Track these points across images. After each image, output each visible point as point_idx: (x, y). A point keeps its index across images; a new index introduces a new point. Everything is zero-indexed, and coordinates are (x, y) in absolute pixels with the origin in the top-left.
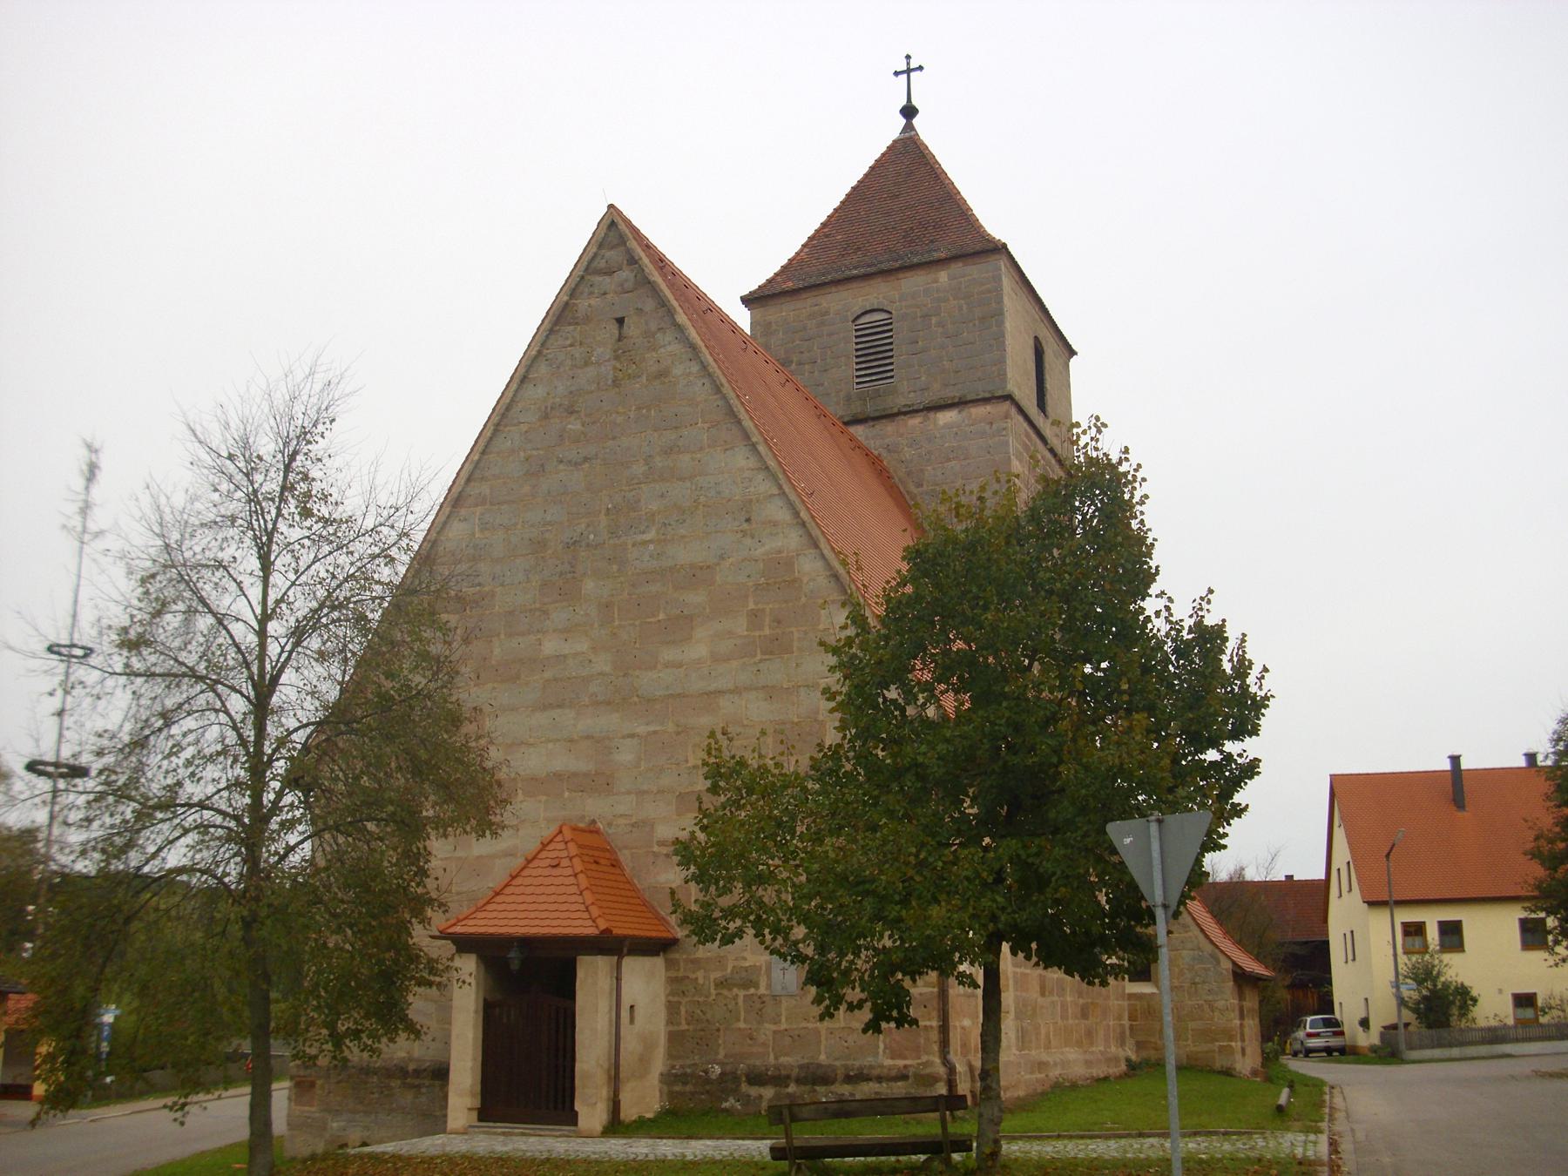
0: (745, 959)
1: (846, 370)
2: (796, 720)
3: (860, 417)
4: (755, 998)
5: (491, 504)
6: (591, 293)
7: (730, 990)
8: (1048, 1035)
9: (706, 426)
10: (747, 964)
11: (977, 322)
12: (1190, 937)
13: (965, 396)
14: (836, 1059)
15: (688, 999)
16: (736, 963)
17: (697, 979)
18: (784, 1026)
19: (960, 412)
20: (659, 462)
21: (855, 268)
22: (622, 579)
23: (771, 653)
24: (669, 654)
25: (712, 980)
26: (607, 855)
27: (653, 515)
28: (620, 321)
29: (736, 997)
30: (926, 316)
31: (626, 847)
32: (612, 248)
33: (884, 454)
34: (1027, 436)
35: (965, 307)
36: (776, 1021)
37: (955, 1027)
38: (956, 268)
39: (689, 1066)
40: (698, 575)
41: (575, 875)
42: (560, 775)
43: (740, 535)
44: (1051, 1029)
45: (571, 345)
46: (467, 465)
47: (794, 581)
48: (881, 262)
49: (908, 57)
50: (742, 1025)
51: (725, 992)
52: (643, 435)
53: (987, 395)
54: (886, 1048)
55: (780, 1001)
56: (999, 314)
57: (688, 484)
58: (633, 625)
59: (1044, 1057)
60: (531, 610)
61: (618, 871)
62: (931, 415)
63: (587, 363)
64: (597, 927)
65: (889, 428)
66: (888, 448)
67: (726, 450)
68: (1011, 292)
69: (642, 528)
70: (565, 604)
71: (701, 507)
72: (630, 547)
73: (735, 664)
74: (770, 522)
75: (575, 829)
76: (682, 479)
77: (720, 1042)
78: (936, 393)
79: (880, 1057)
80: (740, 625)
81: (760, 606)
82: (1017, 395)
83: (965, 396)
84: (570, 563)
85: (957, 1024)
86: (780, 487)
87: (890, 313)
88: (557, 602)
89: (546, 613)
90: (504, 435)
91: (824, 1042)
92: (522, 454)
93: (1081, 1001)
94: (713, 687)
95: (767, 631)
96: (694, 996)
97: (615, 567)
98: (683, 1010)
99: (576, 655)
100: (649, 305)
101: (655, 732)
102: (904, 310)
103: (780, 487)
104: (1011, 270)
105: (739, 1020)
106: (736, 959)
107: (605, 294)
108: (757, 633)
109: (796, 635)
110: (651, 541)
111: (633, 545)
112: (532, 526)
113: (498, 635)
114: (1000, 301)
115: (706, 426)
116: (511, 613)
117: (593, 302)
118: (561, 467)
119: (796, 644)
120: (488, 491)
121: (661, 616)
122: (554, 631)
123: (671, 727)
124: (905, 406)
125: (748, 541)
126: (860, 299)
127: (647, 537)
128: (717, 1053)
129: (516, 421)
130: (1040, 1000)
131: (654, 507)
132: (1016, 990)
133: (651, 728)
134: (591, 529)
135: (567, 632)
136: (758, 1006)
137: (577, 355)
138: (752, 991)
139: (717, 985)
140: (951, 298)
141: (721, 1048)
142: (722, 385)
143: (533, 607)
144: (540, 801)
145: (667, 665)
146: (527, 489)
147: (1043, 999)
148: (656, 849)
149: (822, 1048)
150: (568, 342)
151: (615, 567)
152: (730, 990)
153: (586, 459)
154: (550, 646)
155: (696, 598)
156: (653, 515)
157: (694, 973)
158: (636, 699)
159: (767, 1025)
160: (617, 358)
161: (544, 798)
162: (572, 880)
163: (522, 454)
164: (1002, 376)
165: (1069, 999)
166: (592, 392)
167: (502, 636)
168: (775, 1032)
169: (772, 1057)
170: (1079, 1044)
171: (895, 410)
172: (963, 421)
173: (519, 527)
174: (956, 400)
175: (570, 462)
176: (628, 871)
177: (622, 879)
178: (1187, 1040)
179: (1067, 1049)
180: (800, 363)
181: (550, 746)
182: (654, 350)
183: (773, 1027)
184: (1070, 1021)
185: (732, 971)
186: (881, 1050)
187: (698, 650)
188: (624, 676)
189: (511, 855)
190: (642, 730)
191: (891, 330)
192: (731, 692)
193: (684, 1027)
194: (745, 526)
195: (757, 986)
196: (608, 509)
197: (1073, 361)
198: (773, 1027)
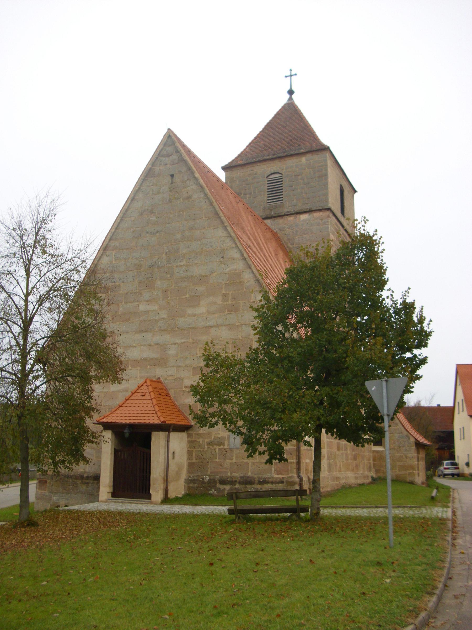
2: (241, 338)
3: (269, 216)
4: (223, 449)
6: (160, 164)
7: (213, 446)
8: (340, 468)
10: (220, 436)
11: (317, 179)
14: (255, 475)
18: (234, 461)
20: (187, 233)
22: (172, 280)
23: (231, 311)
24: (190, 311)
26: (164, 392)
29: (215, 449)
30: (296, 176)
31: (172, 389)
34: (337, 225)
36: (231, 459)
38: (309, 156)
40: (202, 279)
41: (152, 399)
43: (220, 263)
44: (342, 464)
45: (152, 186)
47: (241, 282)
48: (278, 153)
49: (291, 70)
50: (217, 460)
51: (211, 447)
53: (321, 208)
54: (275, 470)
56: (326, 175)
57: (199, 242)
58: (176, 299)
59: (338, 475)
61: (168, 398)
62: (298, 216)
63: (159, 193)
65: (281, 221)
73: (216, 315)
74: (232, 258)
75: (152, 381)
78: (300, 207)
80: (219, 300)
81: (227, 292)
82: (333, 208)
84: (151, 274)
85: (304, 461)
86: (236, 244)
89: (141, 294)
91: (250, 467)
93: (354, 453)
94: (208, 325)
95: (230, 302)
97: (169, 276)
98: (194, 454)
99: (153, 311)
101: (184, 342)
106: (216, 434)
107: (166, 165)
108: (226, 303)
109: (241, 304)
110: (183, 265)
111: (177, 267)
112: (136, 259)
113: (122, 302)
114: (326, 170)
115: (206, 219)
118: (148, 235)
119: (241, 308)
121: (187, 296)
124: (287, 212)
125: (223, 266)
127: (182, 264)
130: (337, 452)
132: (327, 448)
133: (183, 341)
134: (159, 260)
135: (149, 301)
136: (224, 453)
138: (222, 447)
139: (207, 444)
148: (184, 389)
149: (250, 470)
150: (151, 184)
151: (169, 276)
152: (213, 446)
153: (157, 232)
154: (142, 307)
155: (201, 289)
158: (177, 329)
159: (228, 461)
160: (171, 191)
161: (139, 368)
162: (150, 401)
164: (327, 201)
165: (349, 452)
166: (160, 205)
167: (123, 303)
168: (230, 463)
169: (229, 473)
170: (353, 470)
171: (283, 214)
174: (308, 210)
175: (151, 233)
180: (245, 194)
181: (142, 347)
183: (231, 461)
184: (349, 461)
186: (273, 471)
187: (202, 310)
192: (215, 326)
193: (194, 461)
194: (222, 260)
195: (224, 445)
198: (231, 461)
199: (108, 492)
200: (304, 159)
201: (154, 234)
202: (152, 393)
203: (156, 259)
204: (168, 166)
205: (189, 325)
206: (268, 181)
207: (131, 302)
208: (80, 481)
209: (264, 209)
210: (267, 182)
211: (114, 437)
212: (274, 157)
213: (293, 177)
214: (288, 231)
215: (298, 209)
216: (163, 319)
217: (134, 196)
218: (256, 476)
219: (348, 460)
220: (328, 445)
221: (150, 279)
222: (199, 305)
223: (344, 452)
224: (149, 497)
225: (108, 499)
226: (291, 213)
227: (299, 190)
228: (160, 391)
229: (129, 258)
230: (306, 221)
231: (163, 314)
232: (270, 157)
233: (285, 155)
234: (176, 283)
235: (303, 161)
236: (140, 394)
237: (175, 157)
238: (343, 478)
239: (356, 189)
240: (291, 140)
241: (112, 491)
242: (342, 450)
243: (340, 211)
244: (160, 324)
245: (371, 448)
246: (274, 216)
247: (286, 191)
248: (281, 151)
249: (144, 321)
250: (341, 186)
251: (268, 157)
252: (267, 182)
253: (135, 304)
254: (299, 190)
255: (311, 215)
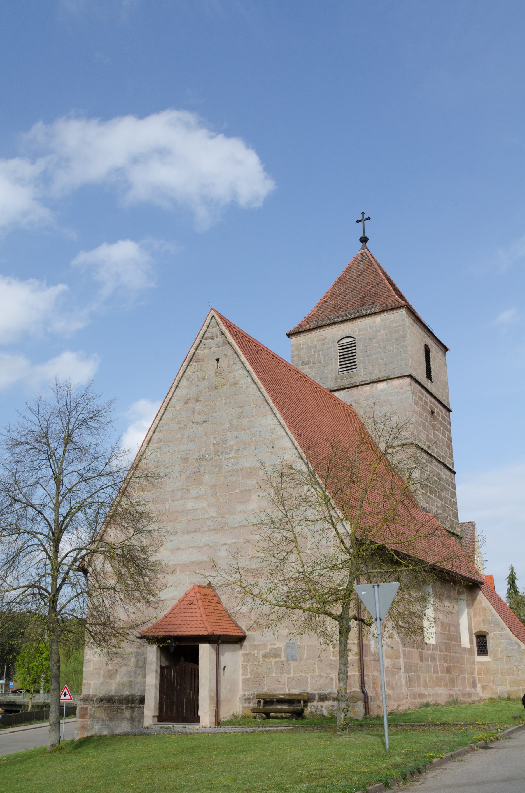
0: (275, 644)
1: (336, 364)
3: (342, 387)
4: (280, 662)
5: (165, 442)
6: (205, 348)
7: (269, 659)
8: (425, 681)
9: (255, 406)
10: (276, 647)
12: (505, 633)
13: (389, 376)
14: (315, 690)
15: (250, 663)
16: (271, 646)
17: (254, 654)
18: (292, 675)
19: (387, 383)
20: (235, 422)
21: (338, 317)
24: (240, 507)
25: (261, 654)
26: (215, 598)
27: (233, 446)
28: (218, 360)
29: (271, 662)
30: (371, 339)
32: (213, 328)
33: (354, 404)
34: (421, 393)
35: (388, 334)
36: (289, 673)
37: (369, 675)
38: (384, 315)
39: (252, 695)
41: (199, 608)
42: (195, 563)
43: (270, 454)
44: (428, 678)
45: (197, 371)
46: (153, 425)
48: (350, 314)
49: (363, 213)
50: (274, 675)
51: (267, 660)
52: (228, 410)
53: (400, 375)
55: (291, 664)
56: (404, 336)
59: (423, 691)
60: (182, 489)
61: (219, 605)
62: (375, 385)
63: (204, 379)
64: (207, 631)
66: (355, 401)
67: (264, 416)
68: (411, 326)
69: (229, 452)
70: (196, 486)
71: (253, 442)
72: (223, 460)
74: (282, 448)
75: (199, 587)
76: (245, 430)
77: (265, 683)
79: (334, 689)
83: (389, 376)
84: (198, 468)
85: (370, 674)
86: (286, 433)
87: (354, 338)
88: (193, 485)
89: (188, 490)
90: (169, 412)
91: (309, 682)
92: (177, 420)
93: (446, 665)
96: (253, 662)
97: (217, 469)
98: (248, 668)
99: (201, 508)
100: (230, 352)
101: (235, 543)
102: (360, 337)
103: (286, 433)
104: (410, 315)
105: (272, 673)
106: (271, 645)
107: (211, 348)
110: (232, 457)
111: (225, 459)
112: (182, 452)
113: (168, 501)
115: (255, 406)
116: (173, 490)
117: (205, 352)
118: (194, 425)
120: (163, 437)
121: (237, 491)
122: (192, 498)
123: (242, 540)
125: (273, 457)
126: (340, 332)
127: (231, 455)
128: (264, 688)
129: (174, 405)
130: (420, 663)
131: (233, 442)
132: (405, 658)
133: (234, 541)
134: (207, 453)
135: (197, 498)
136: (281, 666)
137: (199, 376)
138: (278, 659)
139: (263, 657)
140: (382, 330)
141: (265, 686)
142: (261, 388)
143: (182, 488)
144: (187, 575)
145: (242, 512)
146: (179, 435)
147: (422, 663)
149: (309, 685)
150: (196, 370)
151: (217, 469)
152: (269, 659)
153: (204, 422)
154: (190, 505)
156: (233, 446)
157: (253, 651)
158: (227, 528)
159: (285, 675)
160: (216, 376)
161: (188, 573)
162: (198, 610)
163: (177, 420)
165: (438, 663)
166: (206, 392)
167: (170, 501)
168: (288, 678)
169: (287, 690)
170: (446, 686)
171: (358, 384)
172: (389, 388)
173: (176, 452)
174: (385, 378)
175: (197, 423)
176: (224, 606)
177: (222, 609)
178: (506, 685)
179: (438, 688)
180: (314, 363)
181: (191, 549)
182: (232, 373)
183: (288, 676)
184: (439, 674)
185: (270, 650)
188: (222, 518)
189: (174, 599)
190: (230, 542)
191: (355, 346)
193: (249, 676)
194: (272, 450)
195: (280, 657)
196: (214, 444)
197: (448, 352)
198: (288, 676)
199: (154, 716)
200: (378, 319)
201: (200, 424)
202: (200, 601)
203: (203, 451)
204: (213, 349)
205: (240, 523)
206: (339, 347)
207: (178, 500)
208: (125, 706)
209: (336, 379)
210: (338, 348)
211: (159, 653)
212: (344, 318)
213: (367, 340)
214: (364, 403)
215: (373, 378)
216: (213, 517)
217: (178, 383)
218: (316, 692)
219: (437, 673)
220: (404, 655)
221: (198, 474)
222: (249, 500)
223: (430, 663)
224: (196, 719)
225: (154, 724)
226: (367, 382)
227: (374, 356)
228: (210, 598)
229: (175, 451)
230: (384, 391)
231: (212, 512)
232: (340, 319)
233: (357, 315)
234: (225, 477)
235: (377, 322)
236: (187, 602)
237: (220, 339)
238: (429, 695)
239: (447, 346)
240: (364, 297)
241: (158, 715)
242: (427, 660)
243: (425, 376)
244: (209, 523)
245: (474, 659)
246: (347, 386)
247: (360, 357)
248: (352, 311)
249: (192, 520)
250: (426, 346)
251: (338, 319)
252: (338, 348)
253: (182, 502)
254: (374, 356)
255: (389, 384)
